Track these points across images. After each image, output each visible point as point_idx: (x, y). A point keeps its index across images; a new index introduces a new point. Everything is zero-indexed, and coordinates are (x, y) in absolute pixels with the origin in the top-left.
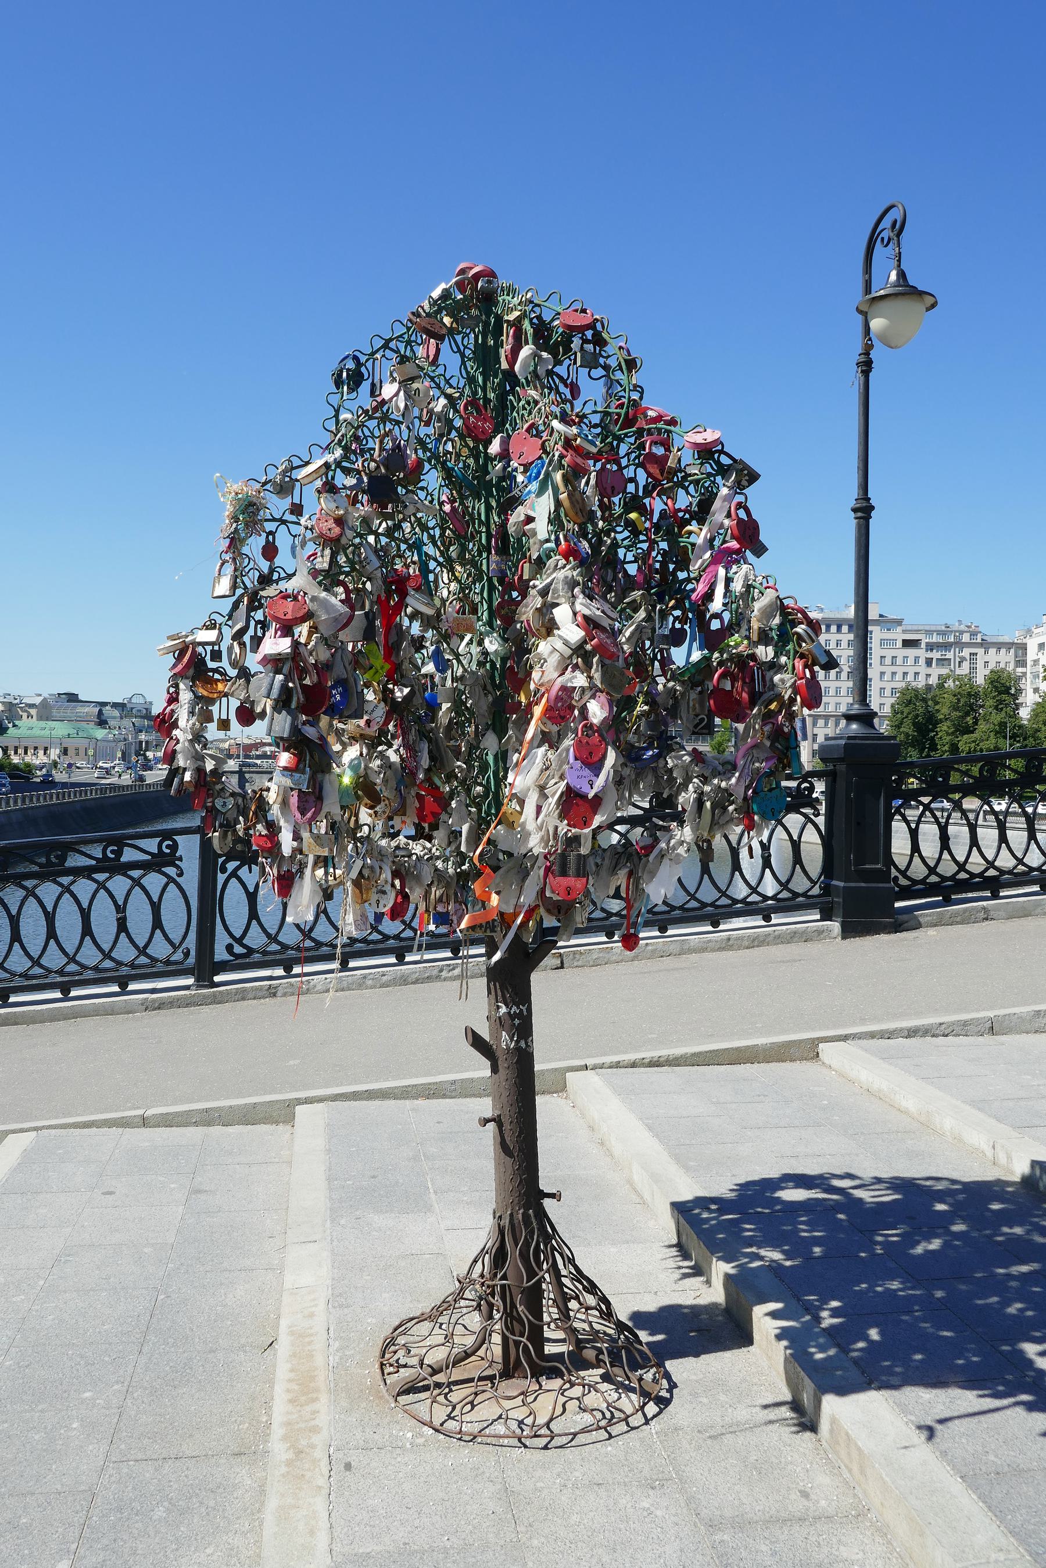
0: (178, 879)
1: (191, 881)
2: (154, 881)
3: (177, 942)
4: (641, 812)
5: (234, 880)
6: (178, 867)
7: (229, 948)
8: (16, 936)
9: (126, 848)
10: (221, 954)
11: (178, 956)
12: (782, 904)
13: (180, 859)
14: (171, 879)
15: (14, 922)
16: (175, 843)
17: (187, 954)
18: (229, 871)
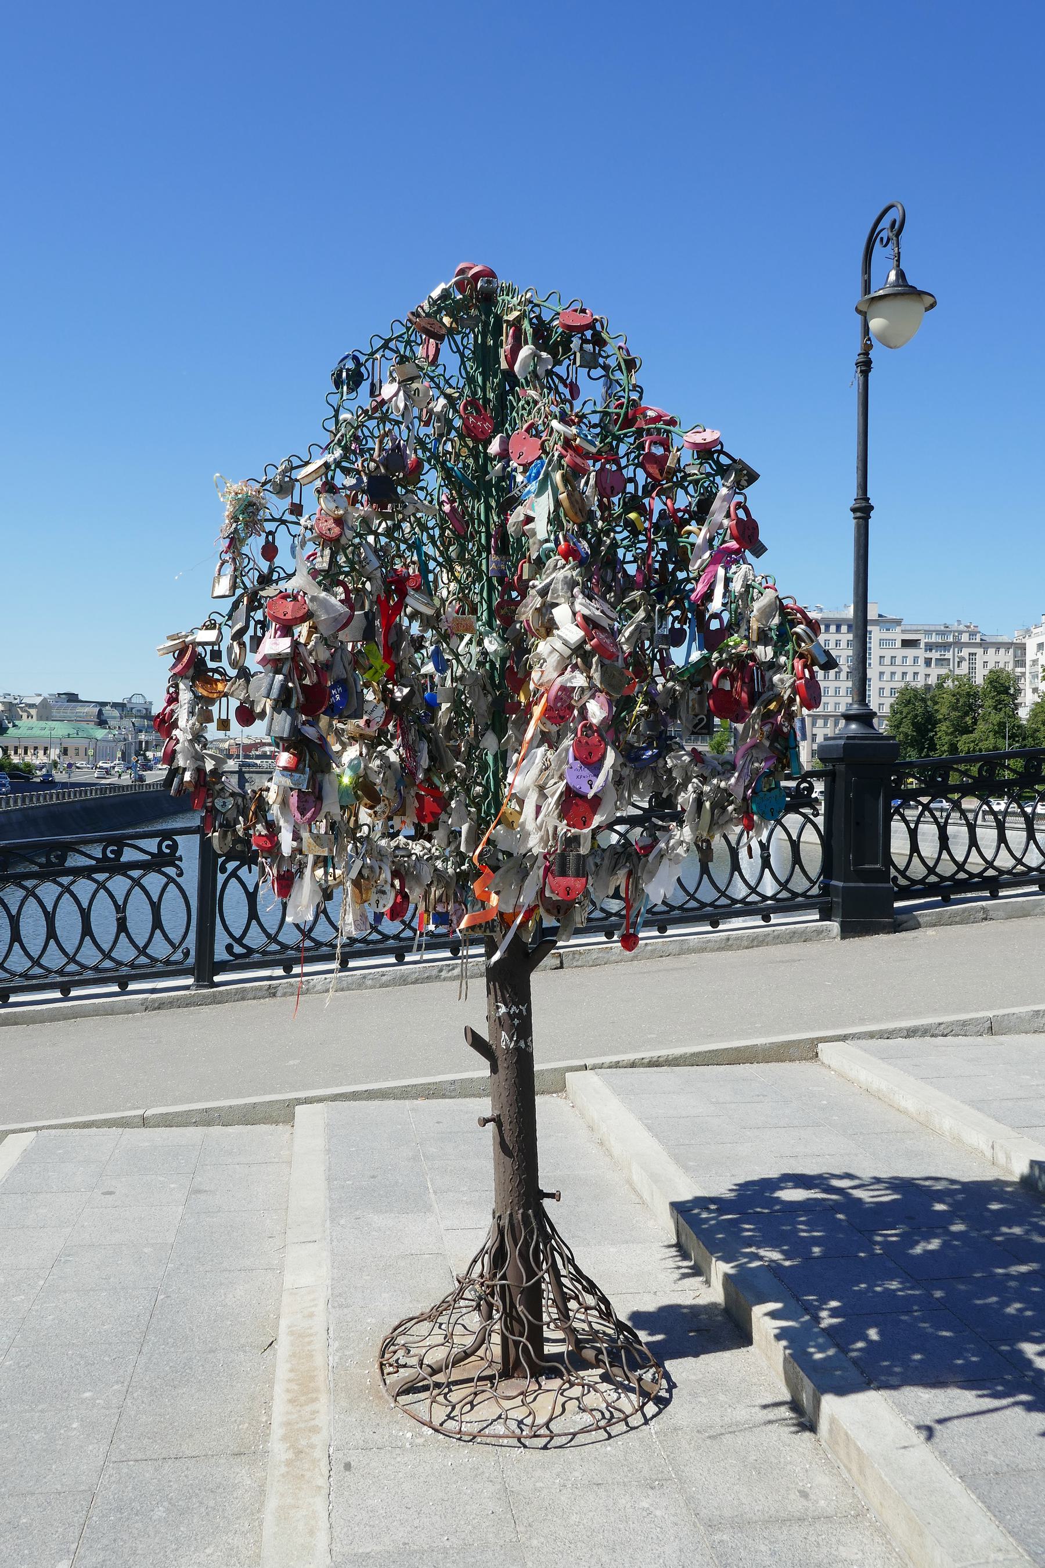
0: (178, 879)
1: (191, 881)
2: (153, 881)
3: (177, 942)
4: (641, 812)
5: (233, 880)
6: (177, 867)
7: (229, 948)
8: (16, 936)
9: (126, 848)
10: (220, 954)
11: (178, 956)
12: (781, 904)
13: (180, 859)
14: (170, 879)
15: (14, 922)
16: (175, 843)
17: (187, 954)
18: (229, 871)
